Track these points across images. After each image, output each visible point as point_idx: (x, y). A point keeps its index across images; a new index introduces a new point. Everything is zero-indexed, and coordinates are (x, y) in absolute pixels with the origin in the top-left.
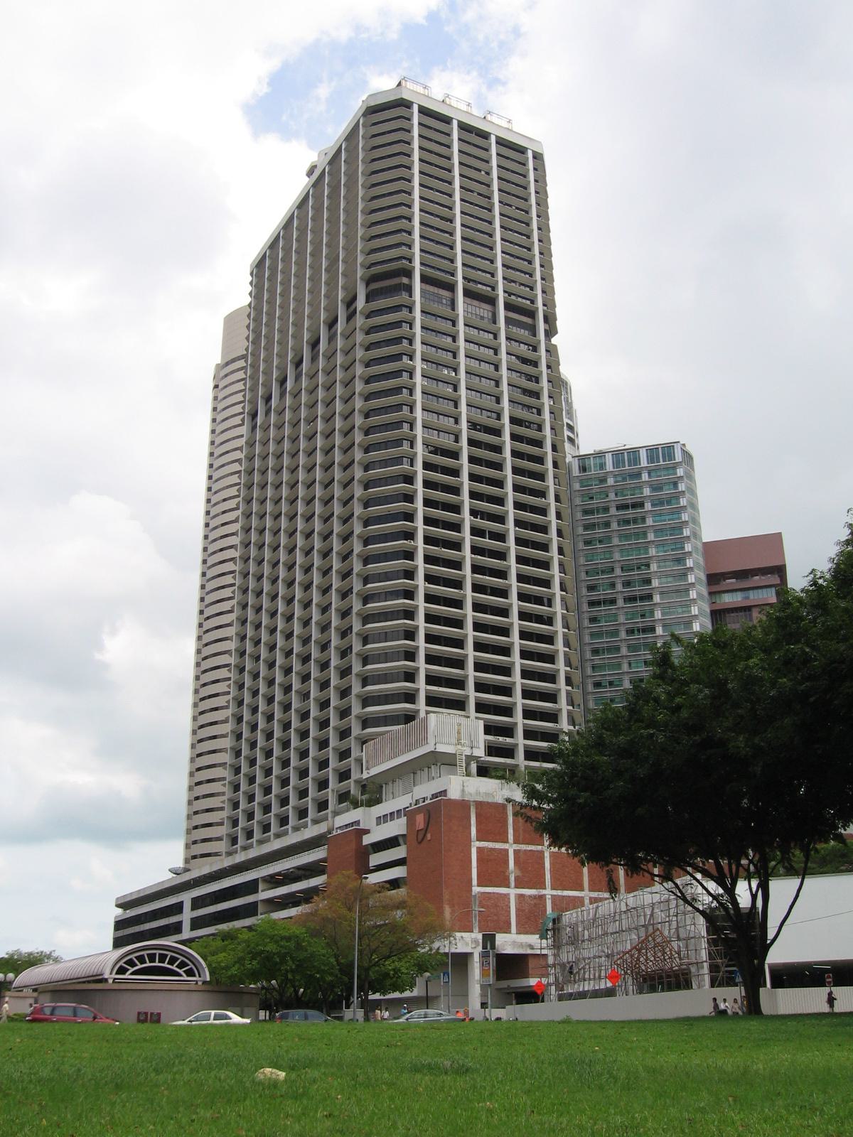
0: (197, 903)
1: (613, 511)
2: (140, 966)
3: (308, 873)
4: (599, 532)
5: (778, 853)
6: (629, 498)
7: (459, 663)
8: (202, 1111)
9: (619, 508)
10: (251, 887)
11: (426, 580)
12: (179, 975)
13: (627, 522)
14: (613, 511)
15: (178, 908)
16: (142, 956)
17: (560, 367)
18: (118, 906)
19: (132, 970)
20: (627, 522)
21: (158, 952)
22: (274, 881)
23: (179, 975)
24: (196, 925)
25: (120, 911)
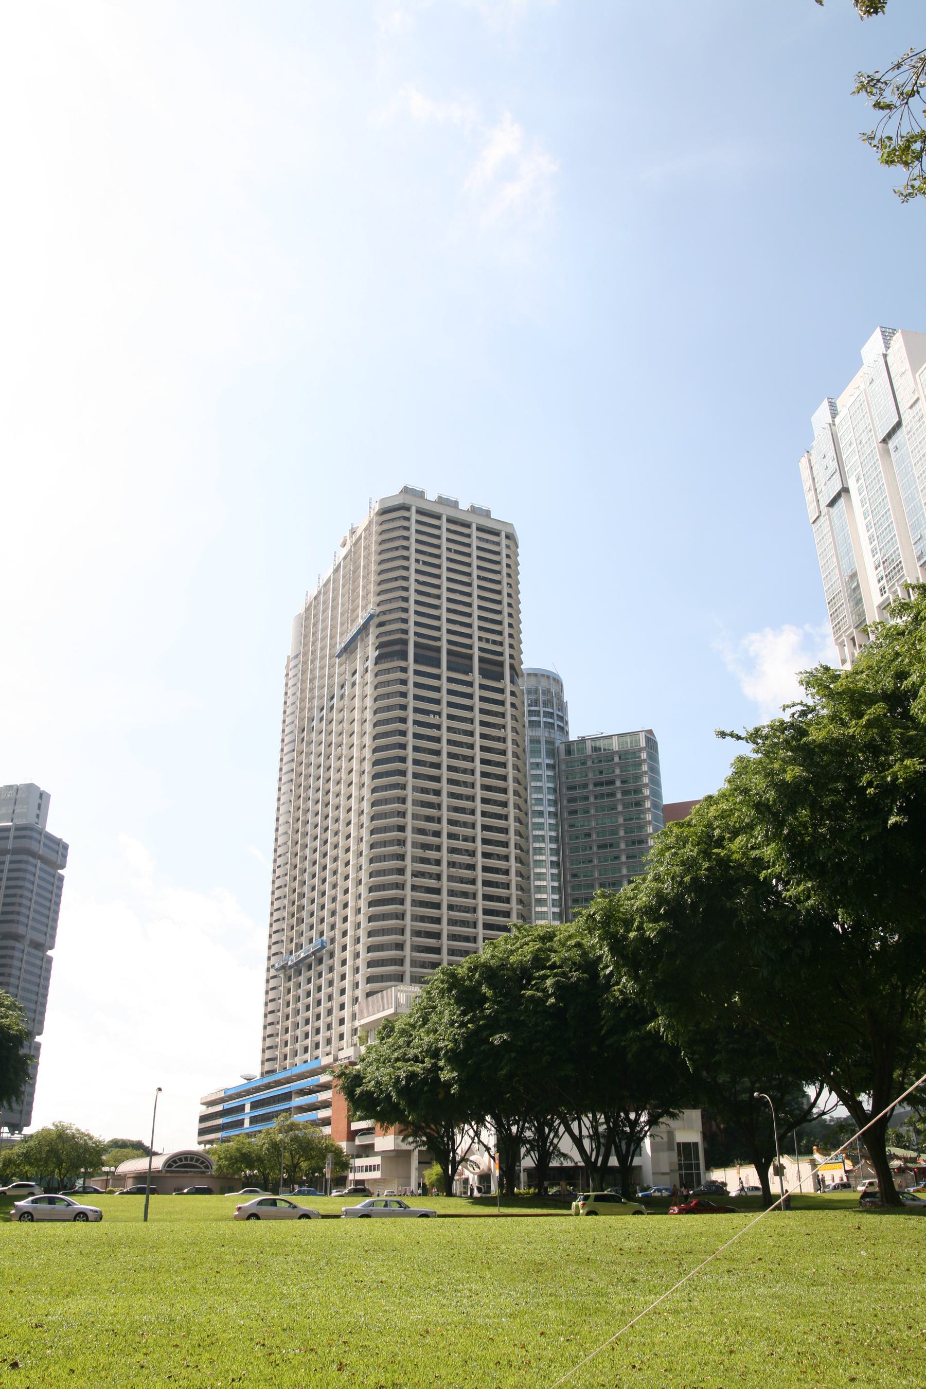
0: (255, 1105)
1: (591, 787)
2: (179, 1163)
3: (324, 1089)
4: (579, 805)
5: (896, 937)
6: (604, 777)
7: (437, 936)
8: (714, 1128)
9: (596, 785)
10: (287, 1097)
11: (448, 823)
12: (200, 1168)
13: (602, 796)
14: (591, 787)
15: (241, 1109)
16: (187, 1158)
17: (521, 646)
18: (203, 1104)
19: (175, 1165)
20: (602, 796)
21: (189, 1156)
22: (302, 1092)
23: (200, 1168)
24: (254, 1120)
25: (204, 1107)
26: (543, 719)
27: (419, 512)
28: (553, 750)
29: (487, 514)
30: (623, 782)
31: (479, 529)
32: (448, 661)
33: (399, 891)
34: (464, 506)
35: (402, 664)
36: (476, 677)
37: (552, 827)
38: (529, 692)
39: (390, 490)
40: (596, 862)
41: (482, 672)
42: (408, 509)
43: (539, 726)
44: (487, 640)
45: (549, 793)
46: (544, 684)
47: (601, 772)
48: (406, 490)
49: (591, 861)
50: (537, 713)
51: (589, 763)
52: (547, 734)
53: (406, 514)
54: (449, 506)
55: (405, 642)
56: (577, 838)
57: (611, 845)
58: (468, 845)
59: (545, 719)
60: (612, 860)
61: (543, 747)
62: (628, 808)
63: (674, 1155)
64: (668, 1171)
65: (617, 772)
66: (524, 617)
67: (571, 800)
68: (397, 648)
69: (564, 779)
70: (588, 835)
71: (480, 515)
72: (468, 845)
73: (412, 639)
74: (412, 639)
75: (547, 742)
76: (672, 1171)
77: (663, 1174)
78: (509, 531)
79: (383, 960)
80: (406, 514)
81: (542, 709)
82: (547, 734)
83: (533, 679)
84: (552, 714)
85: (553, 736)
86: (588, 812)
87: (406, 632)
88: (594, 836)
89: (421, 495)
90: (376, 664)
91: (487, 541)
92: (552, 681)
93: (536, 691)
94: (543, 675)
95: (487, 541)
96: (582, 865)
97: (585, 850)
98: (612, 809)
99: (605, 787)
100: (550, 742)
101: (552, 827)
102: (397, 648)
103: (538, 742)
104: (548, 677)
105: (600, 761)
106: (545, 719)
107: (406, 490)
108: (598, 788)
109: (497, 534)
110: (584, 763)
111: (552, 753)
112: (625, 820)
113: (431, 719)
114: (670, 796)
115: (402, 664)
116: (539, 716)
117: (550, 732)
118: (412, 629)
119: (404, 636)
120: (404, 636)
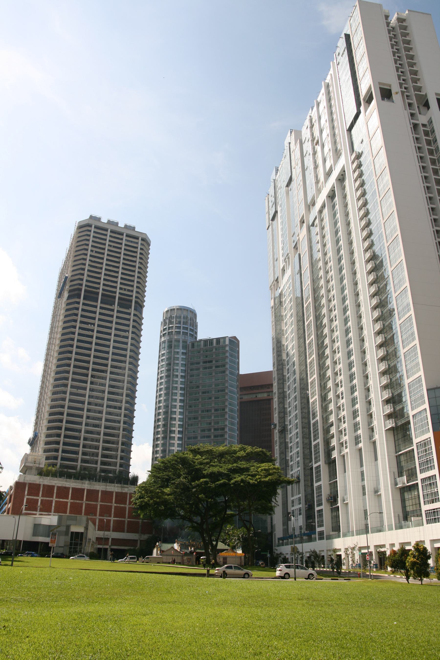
4: (195, 372)
6: (208, 359)
14: (201, 364)
26: (189, 332)
27: (96, 227)
28: (186, 345)
29: (133, 229)
30: (217, 361)
31: (127, 236)
32: (101, 299)
33: (62, 409)
34: (121, 225)
35: (77, 300)
36: (116, 307)
37: (182, 383)
38: (184, 318)
39: (85, 217)
40: (200, 400)
41: (120, 305)
42: (90, 226)
43: (180, 334)
44: (125, 289)
45: (182, 366)
46: (185, 313)
47: (207, 357)
48: (91, 217)
49: (198, 400)
50: (187, 329)
51: (202, 352)
52: (183, 338)
53: (89, 228)
54: (113, 225)
55: (81, 290)
56: (193, 388)
57: (208, 392)
58: (102, 388)
59: (183, 331)
60: (208, 399)
61: (181, 344)
62: (217, 374)
63: (68, 538)
64: (63, 546)
65: (214, 356)
66: (149, 279)
67: (191, 370)
68: (76, 292)
69: (189, 360)
70: (198, 387)
71: (130, 229)
72: (102, 388)
73: (84, 288)
74: (84, 288)
75: (183, 342)
76: (65, 545)
77: (60, 547)
78: (144, 237)
79: (51, 442)
80: (89, 228)
81: (182, 326)
82: (183, 338)
83: (180, 312)
84: (187, 328)
85: (186, 339)
86: (199, 376)
87: (81, 285)
88: (201, 388)
89: (99, 219)
90: (67, 300)
91: (131, 242)
92: (189, 312)
93: (180, 317)
94: (184, 309)
95: (131, 242)
96: (194, 402)
97: (195, 394)
98: (210, 375)
99: (208, 364)
100: (185, 342)
101: (182, 383)
102: (76, 292)
103: (179, 341)
104: (187, 310)
105: (207, 351)
106: (183, 331)
107: (91, 217)
108: (205, 364)
109: (137, 238)
110: (199, 352)
111: (185, 347)
112: (215, 380)
113: (89, 327)
114: (243, 370)
115: (77, 300)
116: (187, 330)
117: (185, 337)
118: (84, 283)
119: (80, 287)
120: (80, 287)
